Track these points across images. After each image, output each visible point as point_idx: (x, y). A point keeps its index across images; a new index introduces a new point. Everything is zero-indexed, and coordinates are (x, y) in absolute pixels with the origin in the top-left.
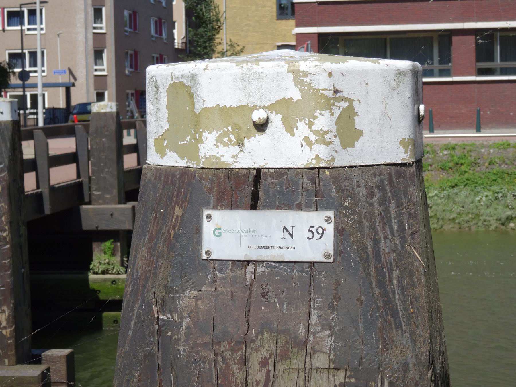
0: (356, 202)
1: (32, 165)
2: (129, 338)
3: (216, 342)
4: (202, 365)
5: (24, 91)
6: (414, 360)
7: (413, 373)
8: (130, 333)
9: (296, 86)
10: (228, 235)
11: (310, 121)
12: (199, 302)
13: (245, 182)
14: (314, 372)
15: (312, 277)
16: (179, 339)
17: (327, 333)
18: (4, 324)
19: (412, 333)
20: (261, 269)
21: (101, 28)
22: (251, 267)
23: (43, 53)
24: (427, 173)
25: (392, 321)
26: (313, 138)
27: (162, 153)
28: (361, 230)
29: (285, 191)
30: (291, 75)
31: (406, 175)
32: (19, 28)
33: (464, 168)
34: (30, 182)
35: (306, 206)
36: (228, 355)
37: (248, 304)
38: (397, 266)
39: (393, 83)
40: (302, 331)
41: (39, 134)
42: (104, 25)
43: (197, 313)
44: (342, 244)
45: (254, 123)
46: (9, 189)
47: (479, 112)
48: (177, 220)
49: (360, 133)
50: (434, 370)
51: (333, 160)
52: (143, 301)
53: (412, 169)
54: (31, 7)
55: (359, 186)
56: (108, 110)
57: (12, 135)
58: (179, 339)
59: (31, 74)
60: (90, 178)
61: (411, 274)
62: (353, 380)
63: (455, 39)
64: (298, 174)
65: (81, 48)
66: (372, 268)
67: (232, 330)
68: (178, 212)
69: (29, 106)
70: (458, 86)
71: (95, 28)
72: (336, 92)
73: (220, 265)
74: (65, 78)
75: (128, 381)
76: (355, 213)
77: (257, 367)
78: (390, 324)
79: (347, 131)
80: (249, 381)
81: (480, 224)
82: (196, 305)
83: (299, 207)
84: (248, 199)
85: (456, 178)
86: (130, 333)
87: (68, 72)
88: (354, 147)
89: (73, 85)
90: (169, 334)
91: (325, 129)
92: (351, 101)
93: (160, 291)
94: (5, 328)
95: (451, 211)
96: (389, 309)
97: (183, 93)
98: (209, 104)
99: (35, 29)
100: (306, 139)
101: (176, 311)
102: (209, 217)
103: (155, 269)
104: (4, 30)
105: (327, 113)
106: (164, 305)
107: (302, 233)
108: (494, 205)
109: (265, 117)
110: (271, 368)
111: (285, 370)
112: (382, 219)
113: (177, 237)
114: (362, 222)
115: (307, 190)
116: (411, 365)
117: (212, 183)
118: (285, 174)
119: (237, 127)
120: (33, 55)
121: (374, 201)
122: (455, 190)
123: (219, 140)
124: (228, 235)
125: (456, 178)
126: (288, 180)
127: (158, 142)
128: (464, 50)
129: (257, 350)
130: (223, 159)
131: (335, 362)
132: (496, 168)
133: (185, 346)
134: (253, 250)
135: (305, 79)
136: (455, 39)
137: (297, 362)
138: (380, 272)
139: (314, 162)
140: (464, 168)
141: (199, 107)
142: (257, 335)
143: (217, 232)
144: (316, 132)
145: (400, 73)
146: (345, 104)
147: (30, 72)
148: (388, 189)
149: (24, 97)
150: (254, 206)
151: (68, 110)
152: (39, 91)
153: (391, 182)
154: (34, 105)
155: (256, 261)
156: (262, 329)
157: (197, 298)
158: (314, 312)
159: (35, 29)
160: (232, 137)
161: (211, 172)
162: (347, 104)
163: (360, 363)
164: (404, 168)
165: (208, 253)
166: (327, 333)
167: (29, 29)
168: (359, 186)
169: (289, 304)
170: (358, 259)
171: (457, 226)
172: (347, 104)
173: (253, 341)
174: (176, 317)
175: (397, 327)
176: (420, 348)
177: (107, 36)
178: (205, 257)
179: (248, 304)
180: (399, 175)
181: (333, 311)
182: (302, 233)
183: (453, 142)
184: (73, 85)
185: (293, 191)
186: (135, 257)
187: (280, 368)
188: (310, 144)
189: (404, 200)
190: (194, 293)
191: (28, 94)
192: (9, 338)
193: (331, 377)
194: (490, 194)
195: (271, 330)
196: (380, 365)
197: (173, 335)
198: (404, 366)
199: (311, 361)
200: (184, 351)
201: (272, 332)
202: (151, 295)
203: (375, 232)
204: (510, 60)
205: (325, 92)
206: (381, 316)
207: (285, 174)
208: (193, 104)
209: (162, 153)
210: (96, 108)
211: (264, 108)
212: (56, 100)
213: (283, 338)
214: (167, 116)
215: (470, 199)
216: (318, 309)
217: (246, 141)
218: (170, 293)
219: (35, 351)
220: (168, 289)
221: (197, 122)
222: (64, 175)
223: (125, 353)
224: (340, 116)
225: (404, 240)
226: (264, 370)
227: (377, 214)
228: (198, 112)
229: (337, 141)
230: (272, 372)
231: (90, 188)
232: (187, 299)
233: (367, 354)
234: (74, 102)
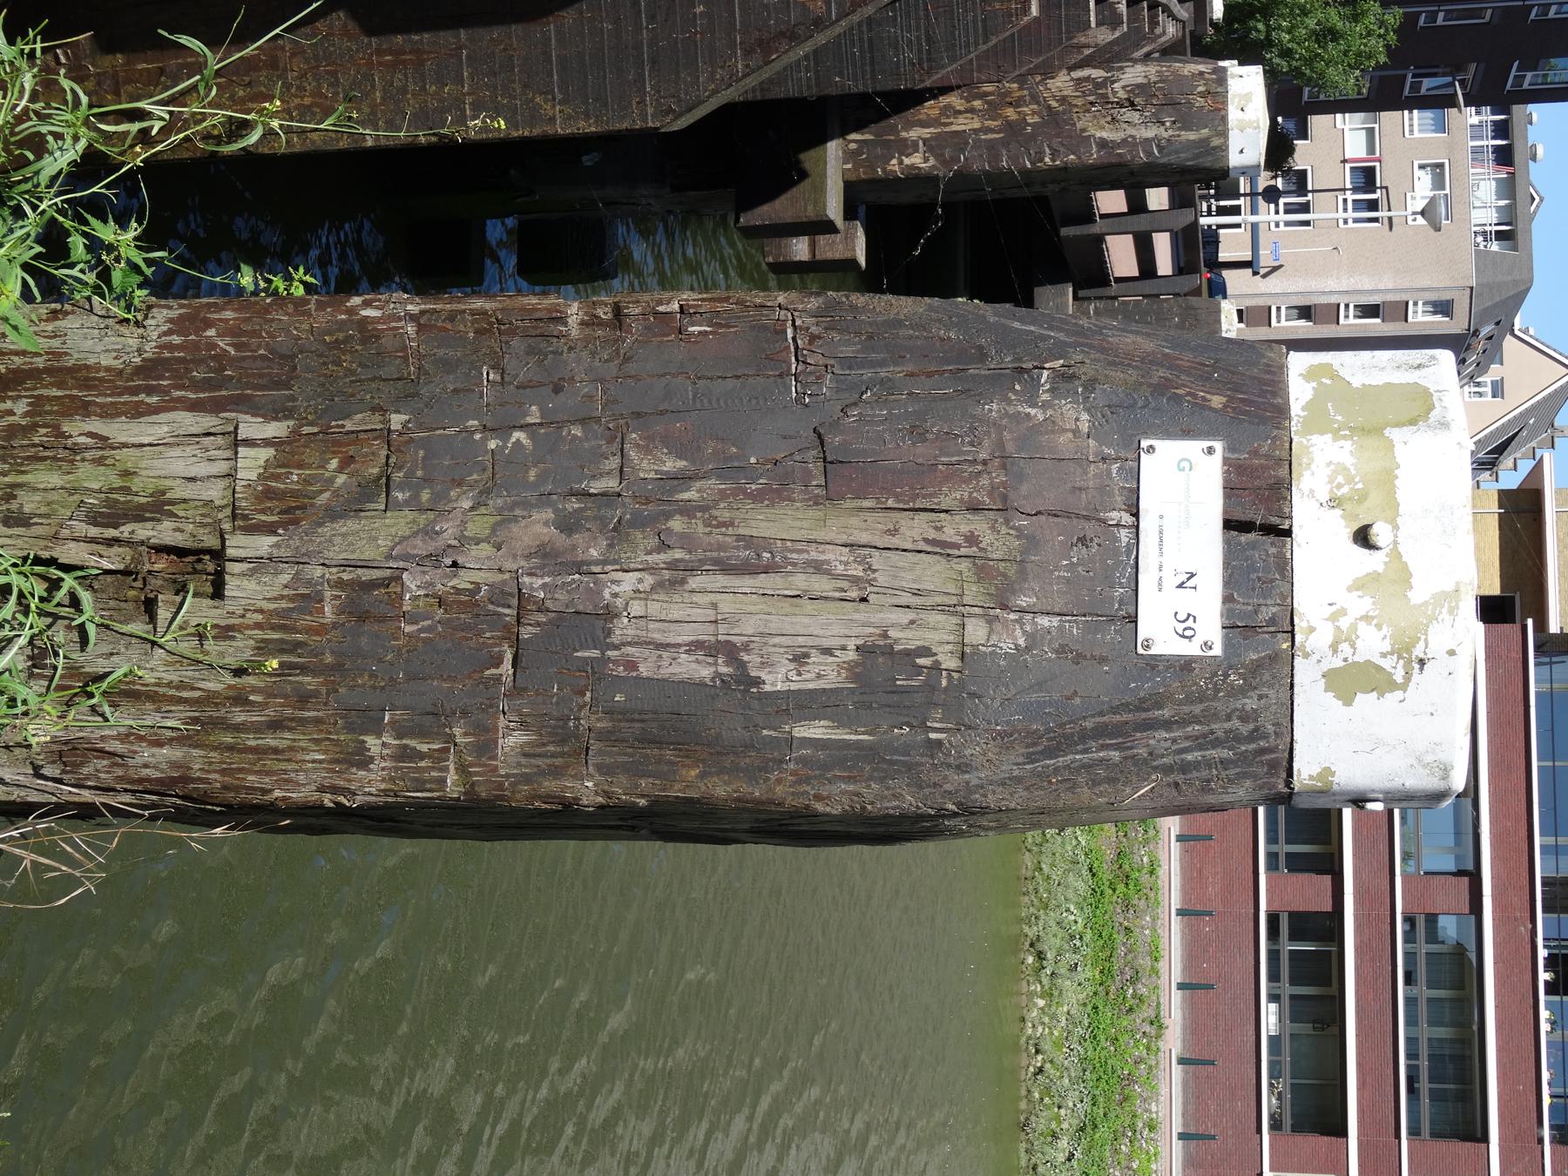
0: (1235, 692)
1: (1137, 205)
2: (1008, 322)
3: (1005, 461)
4: (967, 439)
5: (1245, 195)
6: (975, 782)
7: (955, 780)
8: (1016, 325)
9: (1434, 596)
10: (1181, 483)
11: (1373, 618)
12: (1070, 435)
13: (1269, 510)
14: (955, 620)
15: (1112, 619)
16: (1009, 402)
17: (1021, 642)
18: (907, 161)
19: (1018, 780)
20: (1124, 536)
21: (1347, 317)
22: (1127, 519)
23: (1307, 223)
24: (1114, 829)
25: (1040, 748)
26: (1344, 623)
27: (1310, 374)
28: (1189, 700)
29: (1253, 576)
30: (1450, 587)
31: (1272, 775)
32: (1348, 186)
33: (1121, 888)
34: (1111, 201)
35: (1229, 610)
36: (984, 481)
37: (1068, 515)
38: (1126, 758)
39: (1429, 758)
40: (1023, 601)
41: (1183, 218)
42: (1352, 321)
43: (1053, 432)
44: (1168, 668)
45: (1369, 526)
46: (1119, 165)
47: (1210, 914)
48: (1204, 399)
49: (1348, 702)
50: (955, 815)
51: (1306, 656)
52: (1069, 345)
53: (1281, 787)
54: (1383, 204)
55: (1260, 697)
56: (1224, 326)
57: (1205, 169)
58: (1009, 402)
59: (1272, 206)
60: (1115, 298)
61: (1112, 781)
62: (944, 683)
63: (1327, 879)
64: (1284, 597)
65: (1315, 284)
66: (1126, 717)
67: (1024, 488)
68: (1217, 401)
69: (1222, 203)
70: (1251, 884)
71: (1347, 306)
72: (1422, 662)
73: (1131, 469)
74: (1266, 260)
75: (940, 321)
76: (1217, 690)
77: (964, 529)
78: (1035, 744)
79: (1353, 681)
80: (942, 515)
81: (1032, 910)
82: (1065, 431)
83: (1228, 599)
84: (1239, 516)
85: (1105, 875)
86: (1016, 325)
87: (1276, 264)
88: (1326, 691)
89: (1255, 273)
90: (1017, 387)
91: (1359, 643)
92: (1404, 687)
93: (1087, 371)
94: (901, 162)
95: (1053, 865)
96: (1059, 743)
97: (1417, 408)
98: (1400, 451)
99: (1345, 210)
100: (1343, 612)
101: (1054, 398)
102: (1210, 451)
103: (1122, 364)
104: (1344, 161)
105: (1387, 647)
106: (1064, 378)
107: (1185, 602)
108: (1061, 933)
109: (1379, 544)
110: (963, 551)
111: (961, 573)
112: (1204, 736)
113: (1177, 398)
114: (1201, 701)
115: (1256, 612)
116: (967, 776)
117: (1267, 456)
118: (1283, 577)
119: (1362, 497)
120: (1305, 208)
121: (1235, 723)
122: (1085, 872)
123: (1341, 469)
124: (1181, 483)
125: (1105, 875)
126: (1273, 581)
127: (1327, 369)
128: (1310, 893)
129: (993, 528)
130: (1307, 474)
131: (973, 654)
132: (1120, 938)
133: (999, 411)
134: (1157, 522)
135: (1445, 610)
136: (1327, 879)
137: (973, 593)
138: (1119, 730)
139: (1304, 624)
140: (1121, 888)
141: (1394, 434)
142: (1017, 529)
143: (1186, 464)
144: (1354, 627)
145: (1446, 771)
146: (1399, 676)
147: (1277, 205)
148: (1253, 746)
149: (1237, 196)
150: (1229, 525)
151: (1216, 265)
152: (1245, 217)
153: (1263, 751)
154: (1222, 211)
155: (1137, 527)
156: (1027, 537)
157: (1076, 432)
158: (1055, 621)
159: (1345, 210)
160: (1345, 490)
161: (1285, 455)
162: (1399, 680)
163: (973, 695)
164: (1284, 775)
165: (1151, 449)
166: (1021, 642)
167: (1345, 201)
168: (1260, 697)
169: (1068, 580)
170: (1142, 694)
171: (1029, 874)
172: (1399, 680)
173: (1007, 522)
174: (1046, 397)
175: (1029, 755)
176: (994, 792)
177: (1334, 326)
178: (1145, 444)
179: (1068, 515)
180: (1273, 765)
181: (1057, 652)
182: (1185, 602)
183: (1162, 872)
184: (1255, 273)
185: (1253, 589)
186: (1137, 333)
187: (964, 565)
188: (1334, 618)
189: (1232, 772)
190: (1084, 427)
191: (1241, 201)
192: (884, 170)
193: (950, 647)
194: (1080, 926)
195: (1025, 551)
196: (970, 728)
197: (1016, 392)
198: (967, 765)
199: (975, 616)
200: (990, 411)
201: (1022, 554)
202: (1079, 358)
203: (1184, 722)
204: (1291, 967)
205: (1421, 645)
206: (1049, 730)
207: (1283, 577)
208: (1399, 425)
209: (1310, 374)
210: (1228, 309)
211: (1395, 543)
212: (1232, 247)
213: (1012, 571)
214: (1374, 383)
215: (1070, 894)
216: (1060, 628)
217: (1338, 512)
218: (1085, 388)
219: (862, 210)
220: (1090, 385)
221: (1369, 431)
222: (1121, 256)
223: (984, 316)
224: (1379, 669)
225: (1167, 770)
226: (958, 540)
227: (1214, 726)
228: (1387, 432)
229: (1338, 663)
230: (957, 552)
231: (1100, 298)
232: (1075, 416)
233: (987, 707)
234: (1227, 274)
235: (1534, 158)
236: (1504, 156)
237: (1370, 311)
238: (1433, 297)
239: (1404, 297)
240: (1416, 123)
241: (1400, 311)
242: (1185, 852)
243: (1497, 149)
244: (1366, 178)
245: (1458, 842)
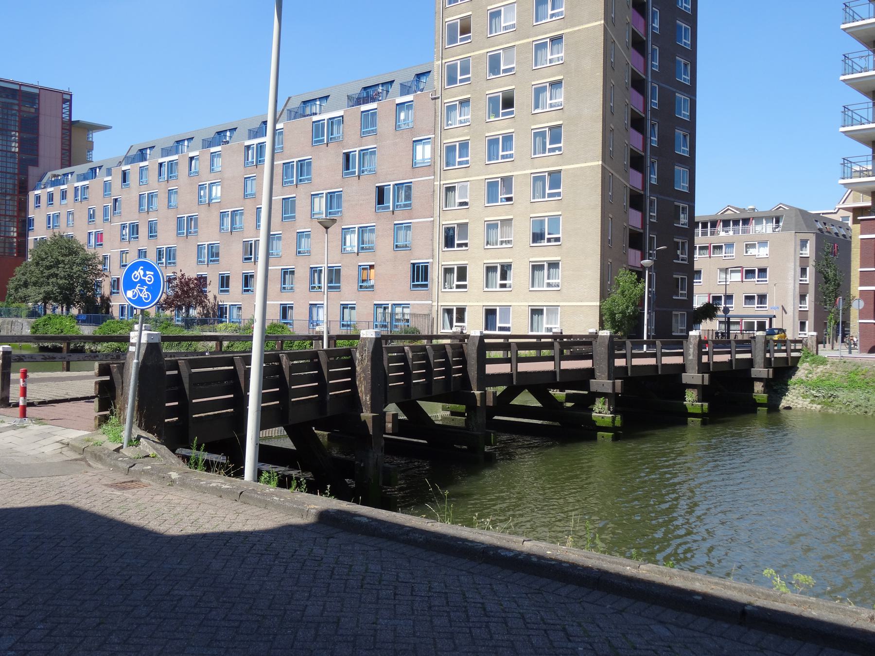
235: (754, 209)
236: (746, 221)
237: (803, 271)
238: (799, 247)
239: (798, 258)
241: (804, 260)
243: (734, 225)
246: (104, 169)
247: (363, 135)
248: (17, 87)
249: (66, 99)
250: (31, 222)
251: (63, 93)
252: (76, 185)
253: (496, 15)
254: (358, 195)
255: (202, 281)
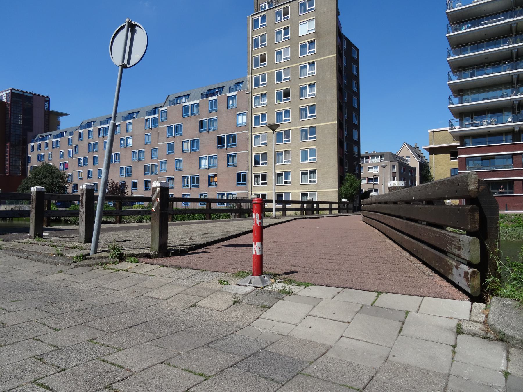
63: (515, 182)
85: (517, 224)
125: (517, 224)
136: (515, 182)
183: (516, 213)
236: (367, 157)
240: (362, 172)
242: (509, 210)
244: (370, 180)
245: (503, 158)
246: (68, 133)
247: (210, 112)
248: (21, 93)
249: (47, 100)
250: (29, 159)
251: (45, 97)
252: (53, 140)
253: (279, 53)
254: (208, 141)
255: (124, 185)
